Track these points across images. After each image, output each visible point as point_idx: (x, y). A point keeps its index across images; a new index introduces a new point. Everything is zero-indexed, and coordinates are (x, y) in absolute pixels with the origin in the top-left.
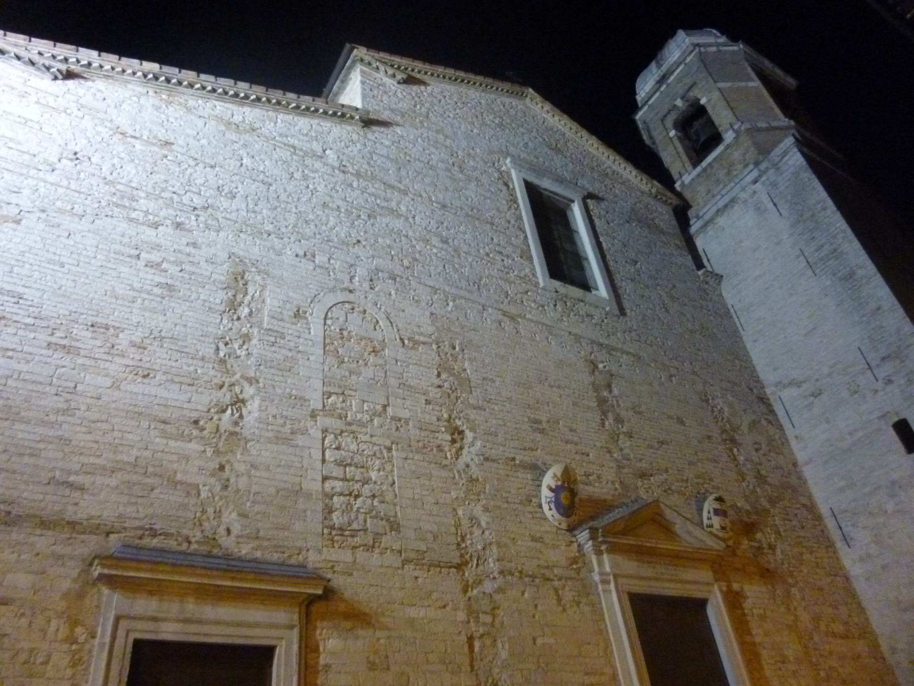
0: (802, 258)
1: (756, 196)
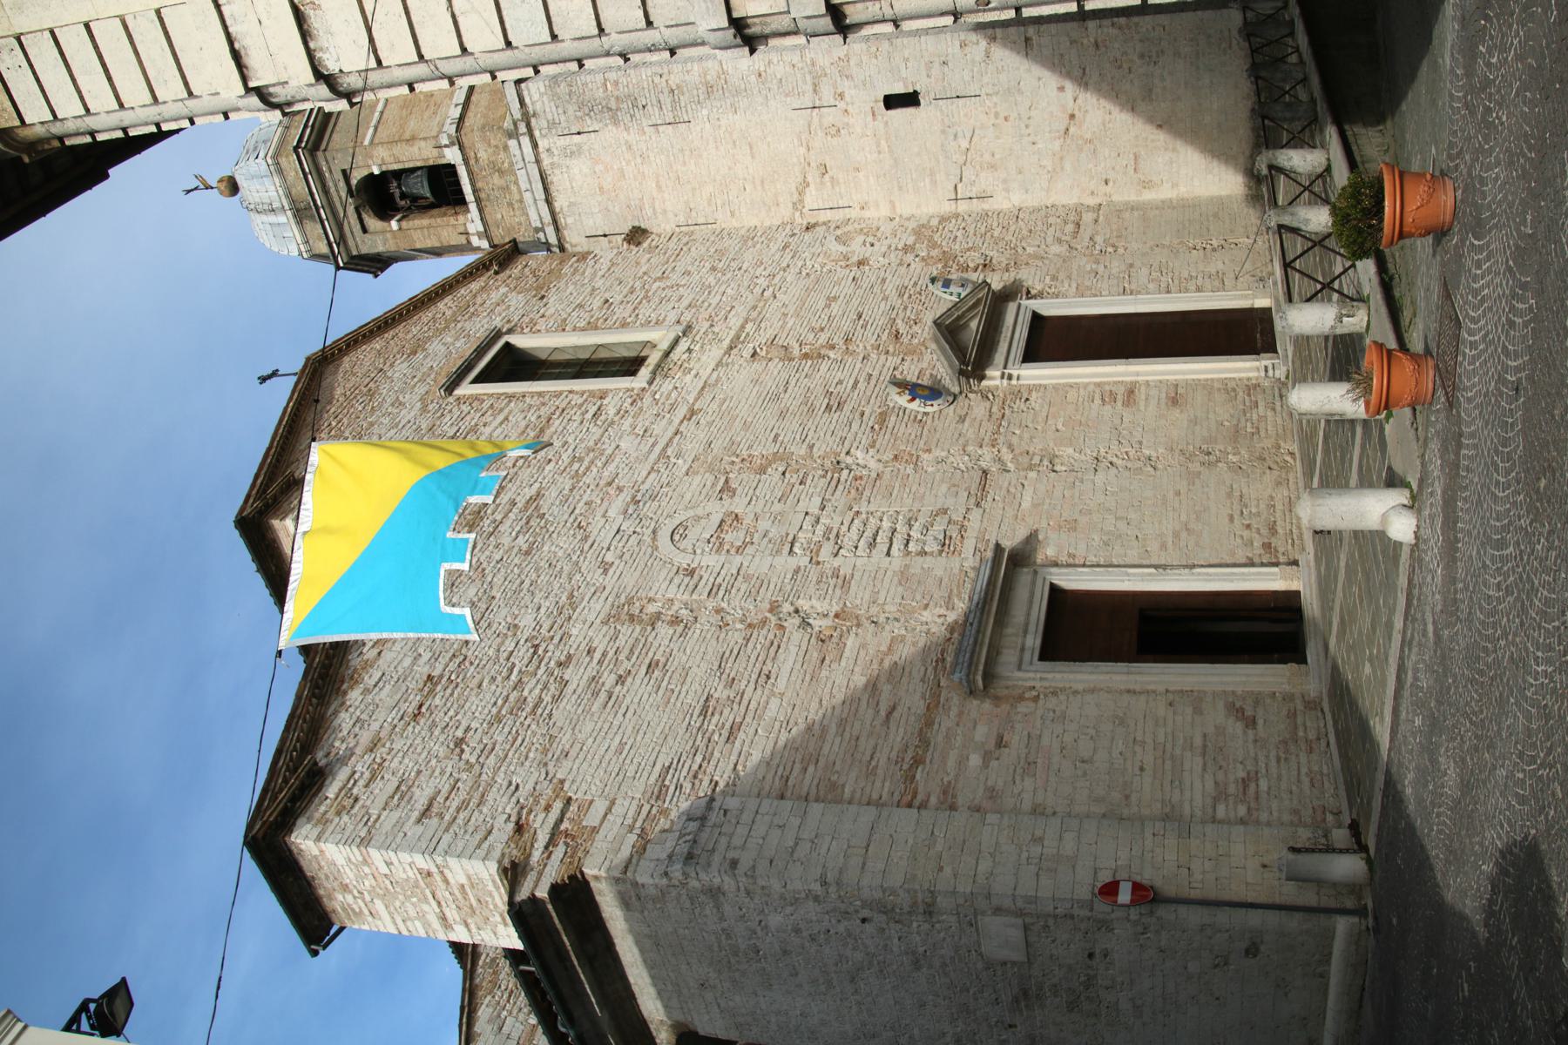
0: (660, 128)
1: (554, 150)
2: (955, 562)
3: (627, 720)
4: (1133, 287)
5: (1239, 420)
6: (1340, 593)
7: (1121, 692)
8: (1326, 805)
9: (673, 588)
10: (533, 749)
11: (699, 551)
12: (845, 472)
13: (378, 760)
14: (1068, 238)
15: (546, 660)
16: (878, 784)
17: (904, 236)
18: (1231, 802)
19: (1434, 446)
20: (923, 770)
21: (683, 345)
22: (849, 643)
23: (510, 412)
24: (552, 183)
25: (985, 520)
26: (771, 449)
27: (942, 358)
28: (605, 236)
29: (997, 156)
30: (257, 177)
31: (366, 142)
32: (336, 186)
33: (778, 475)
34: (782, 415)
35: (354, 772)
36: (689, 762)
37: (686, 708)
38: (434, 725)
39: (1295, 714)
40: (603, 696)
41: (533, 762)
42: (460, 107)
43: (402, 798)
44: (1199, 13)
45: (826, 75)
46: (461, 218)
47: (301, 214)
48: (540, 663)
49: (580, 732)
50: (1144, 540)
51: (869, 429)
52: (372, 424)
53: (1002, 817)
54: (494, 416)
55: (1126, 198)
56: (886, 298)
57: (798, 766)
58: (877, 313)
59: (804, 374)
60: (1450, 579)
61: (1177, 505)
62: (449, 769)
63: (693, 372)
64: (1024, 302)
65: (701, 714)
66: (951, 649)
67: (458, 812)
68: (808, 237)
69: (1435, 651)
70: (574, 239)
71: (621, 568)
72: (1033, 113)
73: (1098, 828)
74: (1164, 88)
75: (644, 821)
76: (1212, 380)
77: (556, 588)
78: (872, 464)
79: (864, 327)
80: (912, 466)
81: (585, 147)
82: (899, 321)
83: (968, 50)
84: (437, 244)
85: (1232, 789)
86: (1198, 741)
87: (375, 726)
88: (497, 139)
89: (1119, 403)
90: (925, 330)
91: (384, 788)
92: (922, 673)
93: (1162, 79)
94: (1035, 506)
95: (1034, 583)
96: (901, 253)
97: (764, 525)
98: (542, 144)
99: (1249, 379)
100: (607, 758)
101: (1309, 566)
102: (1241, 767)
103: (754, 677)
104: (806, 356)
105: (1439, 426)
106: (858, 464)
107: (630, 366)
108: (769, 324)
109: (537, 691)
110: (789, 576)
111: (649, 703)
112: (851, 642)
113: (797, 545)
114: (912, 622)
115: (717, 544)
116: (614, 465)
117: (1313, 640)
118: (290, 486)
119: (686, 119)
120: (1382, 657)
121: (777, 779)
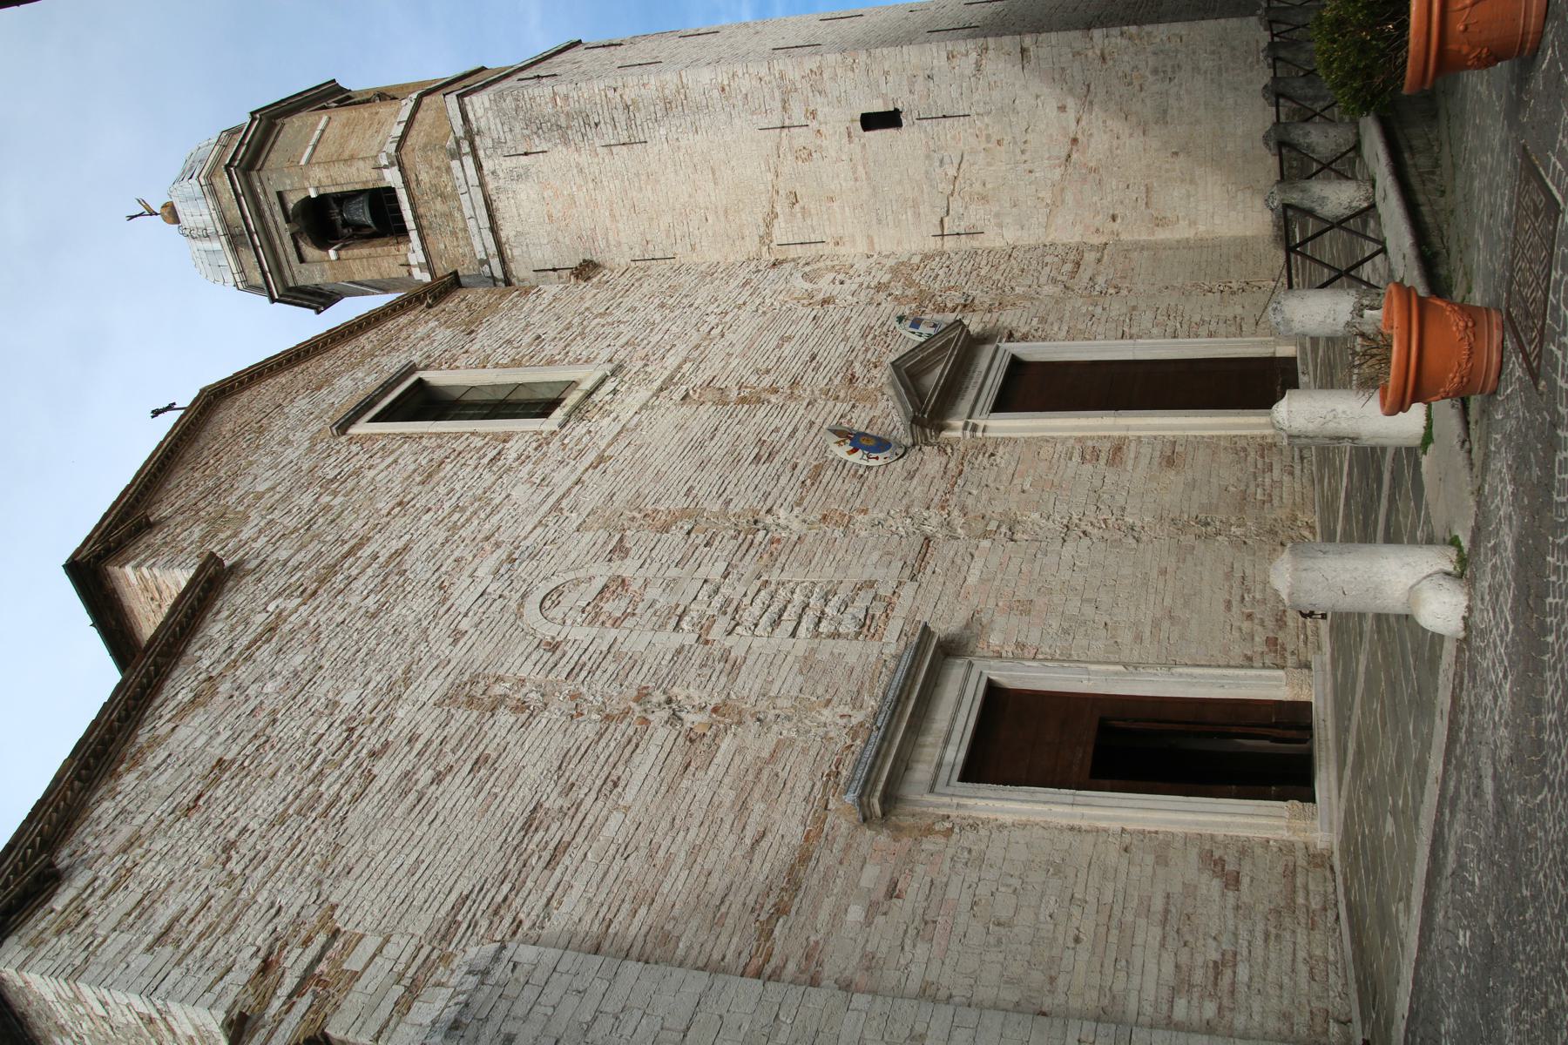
0: (615, 149)
2: (873, 647)
3: (432, 831)
4: (1134, 330)
5: (1247, 486)
6: (1357, 711)
7: (1061, 830)
8: (1330, 1008)
9: (529, 664)
10: (312, 861)
11: (569, 622)
12: (762, 533)
13: (129, 864)
14: (1064, 278)
15: (358, 747)
16: (724, 939)
17: (880, 274)
18: (1196, 995)
19: (1501, 463)
20: (785, 923)
21: (609, 386)
22: (724, 746)
23: (402, 454)
24: (497, 209)
25: (919, 597)
26: (682, 503)
27: (899, 406)
28: (554, 270)
29: (989, 186)
30: (191, 199)
31: (303, 162)
32: (271, 209)
33: (681, 535)
34: (702, 466)
35: (95, 879)
36: (493, 891)
37: (507, 817)
38: (207, 822)
39: (1294, 872)
40: (412, 797)
41: (307, 878)
42: (403, 125)
43: (139, 916)
44: (1222, 21)
45: (796, 90)
46: (403, 248)
47: (235, 241)
48: (350, 751)
49: (373, 842)
50: (1115, 629)
51: (799, 483)
52: (251, 463)
53: (873, 1000)
54: (383, 458)
55: (1136, 237)
56: (846, 339)
57: (626, 906)
58: (834, 354)
59: (737, 420)
60: (1530, 703)
61: (1161, 586)
62: (207, 881)
63: (613, 415)
64: (1004, 345)
65: (522, 828)
66: (849, 760)
67: (199, 940)
68: (772, 274)
69: (1497, 828)
70: (520, 270)
71: (474, 638)
72: (1029, 137)
73: (1003, 1025)
74: (1181, 109)
75: (419, 968)
76: (1219, 437)
77: (394, 659)
78: (796, 525)
79: (815, 369)
80: (841, 529)
81: (533, 170)
82: (857, 365)
83: (956, 62)
84: (377, 277)
85: (1198, 977)
86: (1158, 904)
87: (140, 819)
88: (439, 159)
89: (1102, 462)
90: (883, 375)
91: (123, 901)
92: (808, 789)
93: (1179, 98)
94: (982, 581)
95: (966, 679)
96: (872, 291)
97: (652, 593)
98: (487, 165)
99: (1263, 437)
100: (395, 880)
101: (1324, 671)
102: (1214, 944)
103: (599, 783)
104: (743, 400)
105: (1511, 425)
106: (778, 525)
107: (544, 408)
108: (709, 364)
109: (337, 786)
110: (668, 657)
111: (463, 811)
112: (726, 744)
113: (687, 619)
114: (807, 721)
115: (593, 614)
116: (498, 517)
117: (1323, 770)
118: (140, 529)
119: (642, 139)
120: (1410, 813)
121: (597, 922)
